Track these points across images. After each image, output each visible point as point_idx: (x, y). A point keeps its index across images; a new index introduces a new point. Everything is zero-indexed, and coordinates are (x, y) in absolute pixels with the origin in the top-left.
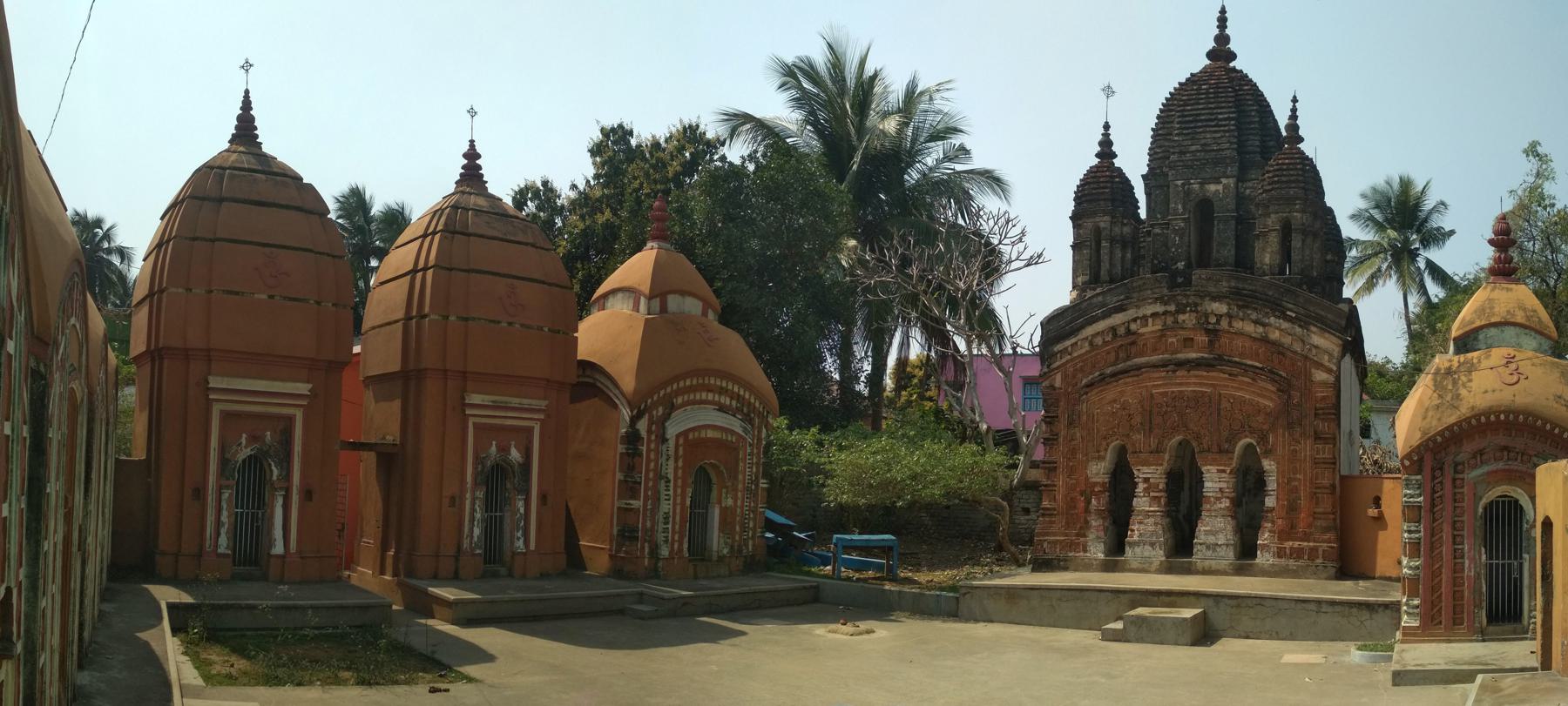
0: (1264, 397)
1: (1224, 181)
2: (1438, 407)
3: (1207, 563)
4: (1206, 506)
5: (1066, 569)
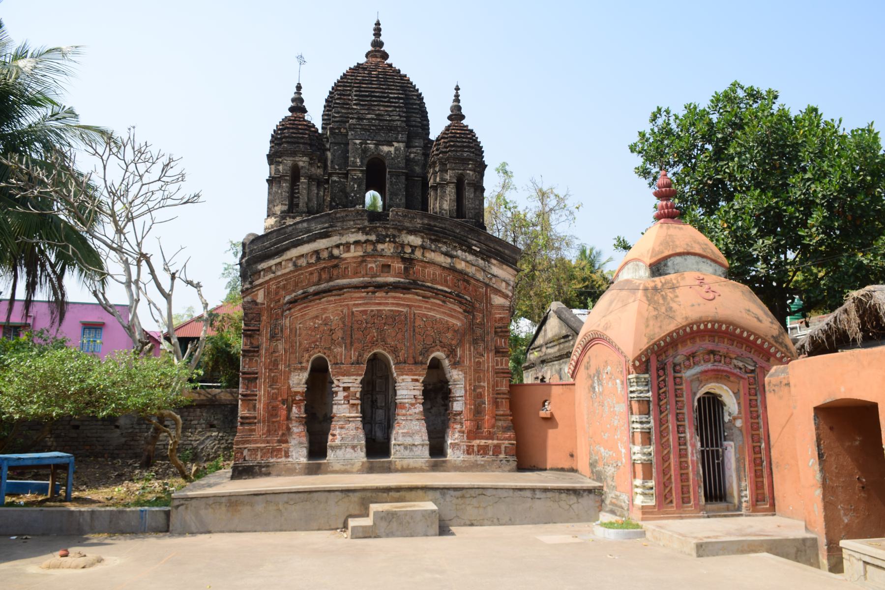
0: (452, 316)
1: (396, 144)
2: (656, 317)
3: (405, 463)
4: (398, 411)
5: (268, 474)
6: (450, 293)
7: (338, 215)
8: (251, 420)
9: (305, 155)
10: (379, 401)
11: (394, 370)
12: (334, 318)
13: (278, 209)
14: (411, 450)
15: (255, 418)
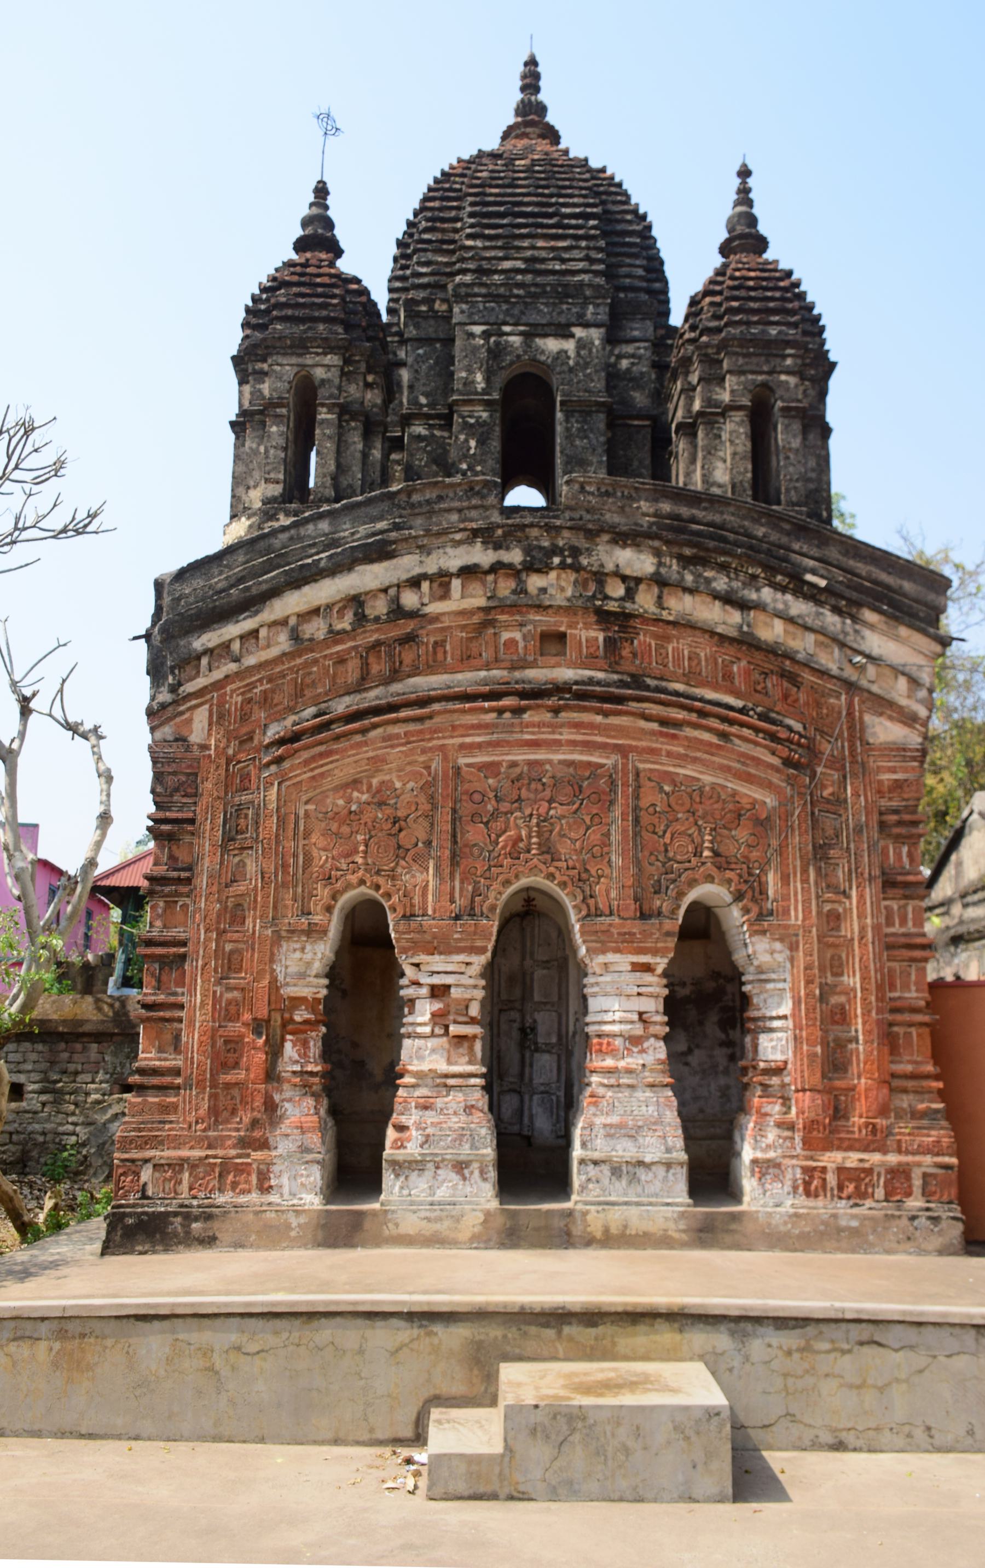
1: (579, 332)
3: (615, 1217)
4: (595, 1061)
5: (209, 1241)
6: (742, 711)
7: (416, 498)
8: (167, 1080)
9: (329, 348)
10: (541, 1029)
11: (578, 936)
12: (406, 787)
13: (255, 498)
14: (634, 1179)
15: (177, 1072)
